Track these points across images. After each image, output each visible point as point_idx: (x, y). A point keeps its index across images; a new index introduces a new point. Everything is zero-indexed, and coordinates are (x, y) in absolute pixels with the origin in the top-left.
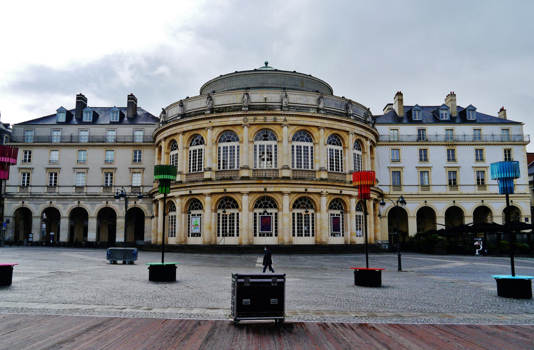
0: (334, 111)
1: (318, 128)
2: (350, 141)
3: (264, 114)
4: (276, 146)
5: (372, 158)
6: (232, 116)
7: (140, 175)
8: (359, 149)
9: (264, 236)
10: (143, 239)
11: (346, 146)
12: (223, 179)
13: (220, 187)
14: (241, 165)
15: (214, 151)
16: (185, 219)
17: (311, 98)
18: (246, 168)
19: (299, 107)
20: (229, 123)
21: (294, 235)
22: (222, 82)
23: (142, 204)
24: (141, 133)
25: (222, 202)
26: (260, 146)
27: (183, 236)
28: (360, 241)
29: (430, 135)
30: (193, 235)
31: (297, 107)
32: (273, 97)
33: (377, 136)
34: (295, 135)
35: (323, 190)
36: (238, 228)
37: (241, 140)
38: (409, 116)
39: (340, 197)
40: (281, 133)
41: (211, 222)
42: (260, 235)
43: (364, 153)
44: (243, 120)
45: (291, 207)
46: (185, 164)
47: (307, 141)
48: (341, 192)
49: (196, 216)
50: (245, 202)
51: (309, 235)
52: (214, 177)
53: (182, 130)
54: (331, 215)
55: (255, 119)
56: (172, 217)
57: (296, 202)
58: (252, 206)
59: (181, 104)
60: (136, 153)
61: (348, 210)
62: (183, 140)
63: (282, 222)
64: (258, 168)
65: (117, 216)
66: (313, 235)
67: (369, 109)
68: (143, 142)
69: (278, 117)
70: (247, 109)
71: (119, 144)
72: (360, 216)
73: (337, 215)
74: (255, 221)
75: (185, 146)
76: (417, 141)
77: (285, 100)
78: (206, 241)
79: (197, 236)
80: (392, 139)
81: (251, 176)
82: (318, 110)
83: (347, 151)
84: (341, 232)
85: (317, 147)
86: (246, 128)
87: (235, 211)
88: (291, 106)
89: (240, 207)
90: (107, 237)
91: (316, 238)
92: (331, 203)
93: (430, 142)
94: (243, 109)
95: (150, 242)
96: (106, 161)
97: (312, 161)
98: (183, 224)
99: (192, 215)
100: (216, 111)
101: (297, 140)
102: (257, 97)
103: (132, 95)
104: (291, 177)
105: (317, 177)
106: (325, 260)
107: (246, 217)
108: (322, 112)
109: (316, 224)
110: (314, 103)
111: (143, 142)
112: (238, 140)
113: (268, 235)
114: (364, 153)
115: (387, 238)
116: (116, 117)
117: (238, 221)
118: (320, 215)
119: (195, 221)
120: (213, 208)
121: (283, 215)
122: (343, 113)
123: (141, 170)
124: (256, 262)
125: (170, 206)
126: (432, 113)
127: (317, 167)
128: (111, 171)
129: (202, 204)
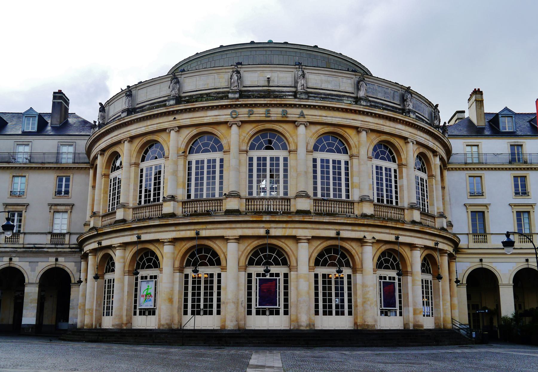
0: (383, 104)
1: (358, 130)
2: (410, 154)
3: (266, 105)
4: (285, 159)
5: (443, 188)
6: (212, 108)
7: (66, 216)
8: (422, 169)
9: (264, 313)
10: (68, 321)
11: (404, 162)
12: (196, 214)
13: (189, 227)
14: (226, 191)
15: (181, 167)
16: (129, 285)
17: (345, 80)
18: (235, 195)
19: (324, 94)
20: (206, 120)
21: (317, 313)
22: (199, 63)
23: (68, 264)
24: (71, 149)
25: (192, 255)
26: (259, 159)
27: (125, 313)
28: (428, 324)
29: (530, 154)
30: (143, 312)
31: (321, 94)
32: (283, 78)
33: (448, 152)
34: (319, 141)
35: (366, 234)
36: (219, 300)
37: (226, 148)
38: (493, 126)
39: (396, 247)
40: (295, 137)
41: (172, 290)
42: (258, 313)
43: (431, 176)
44: (231, 115)
45: (312, 264)
46: (132, 191)
47: (339, 152)
48: (397, 238)
49: (148, 279)
50: (233, 254)
51: (343, 314)
52: (179, 211)
53: (128, 135)
54: (381, 278)
55: (251, 113)
56: (110, 281)
57: (321, 255)
58: (243, 262)
59: (129, 92)
60: (61, 180)
61: (409, 269)
62: (130, 151)
63: (297, 288)
64: (255, 195)
65: (26, 281)
66: (350, 313)
67: (437, 105)
68: (74, 163)
69: (290, 110)
70: (237, 96)
71: (35, 166)
72: (427, 282)
73: (390, 278)
74: (250, 288)
75: (133, 161)
76: (510, 163)
77: (301, 82)
78: (163, 322)
79: (149, 314)
80: (469, 161)
81: (243, 208)
82: (357, 100)
83: (404, 170)
84: (397, 308)
85: (355, 161)
86: (234, 128)
87: (214, 270)
88: (311, 93)
89: (223, 263)
90: (12, 316)
91: (356, 318)
92: (379, 258)
93: (531, 164)
94: (230, 95)
95: (76, 324)
96: (12, 194)
97: (347, 185)
98: (126, 293)
99: (142, 278)
100: (184, 101)
101: (322, 150)
102: (253, 78)
103: (60, 92)
104: (312, 211)
105: (357, 212)
106: (379, 359)
107: (233, 280)
108: (363, 103)
109: (356, 294)
110: (350, 89)
111: (74, 163)
112: (221, 148)
113: (271, 313)
114: (431, 176)
115: (465, 320)
116: (33, 124)
117: (219, 288)
118: (363, 278)
119: (145, 288)
120: (177, 264)
121: (298, 277)
122: (396, 108)
123: (69, 207)
124: (248, 365)
125: (107, 264)
126: (529, 122)
127: (355, 196)
128: (19, 208)
129: (158, 259)
